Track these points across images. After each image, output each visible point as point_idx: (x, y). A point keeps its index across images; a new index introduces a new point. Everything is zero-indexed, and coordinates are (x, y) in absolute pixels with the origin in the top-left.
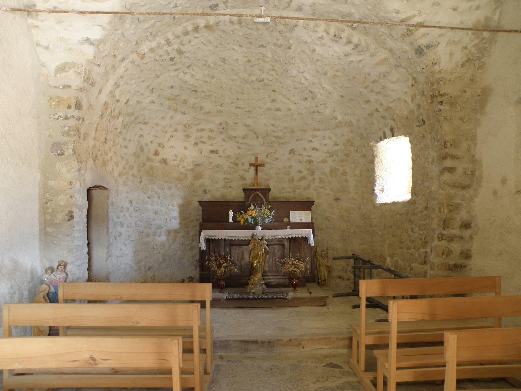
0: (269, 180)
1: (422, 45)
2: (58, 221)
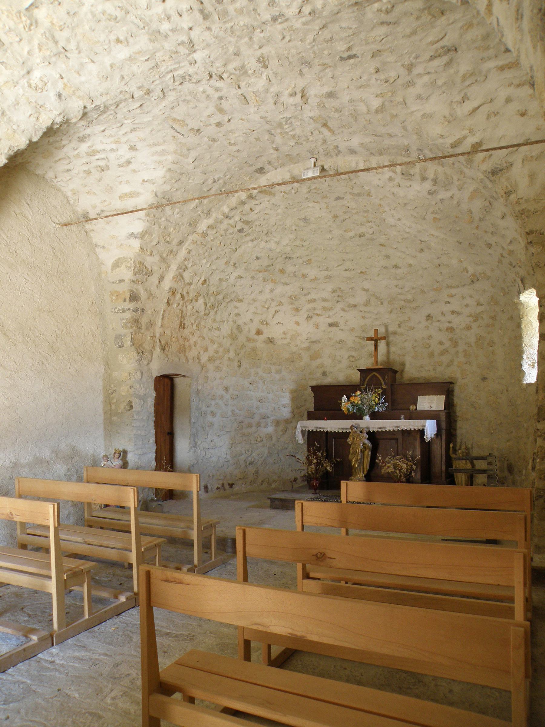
0: (404, 355)
2: (120, 411)
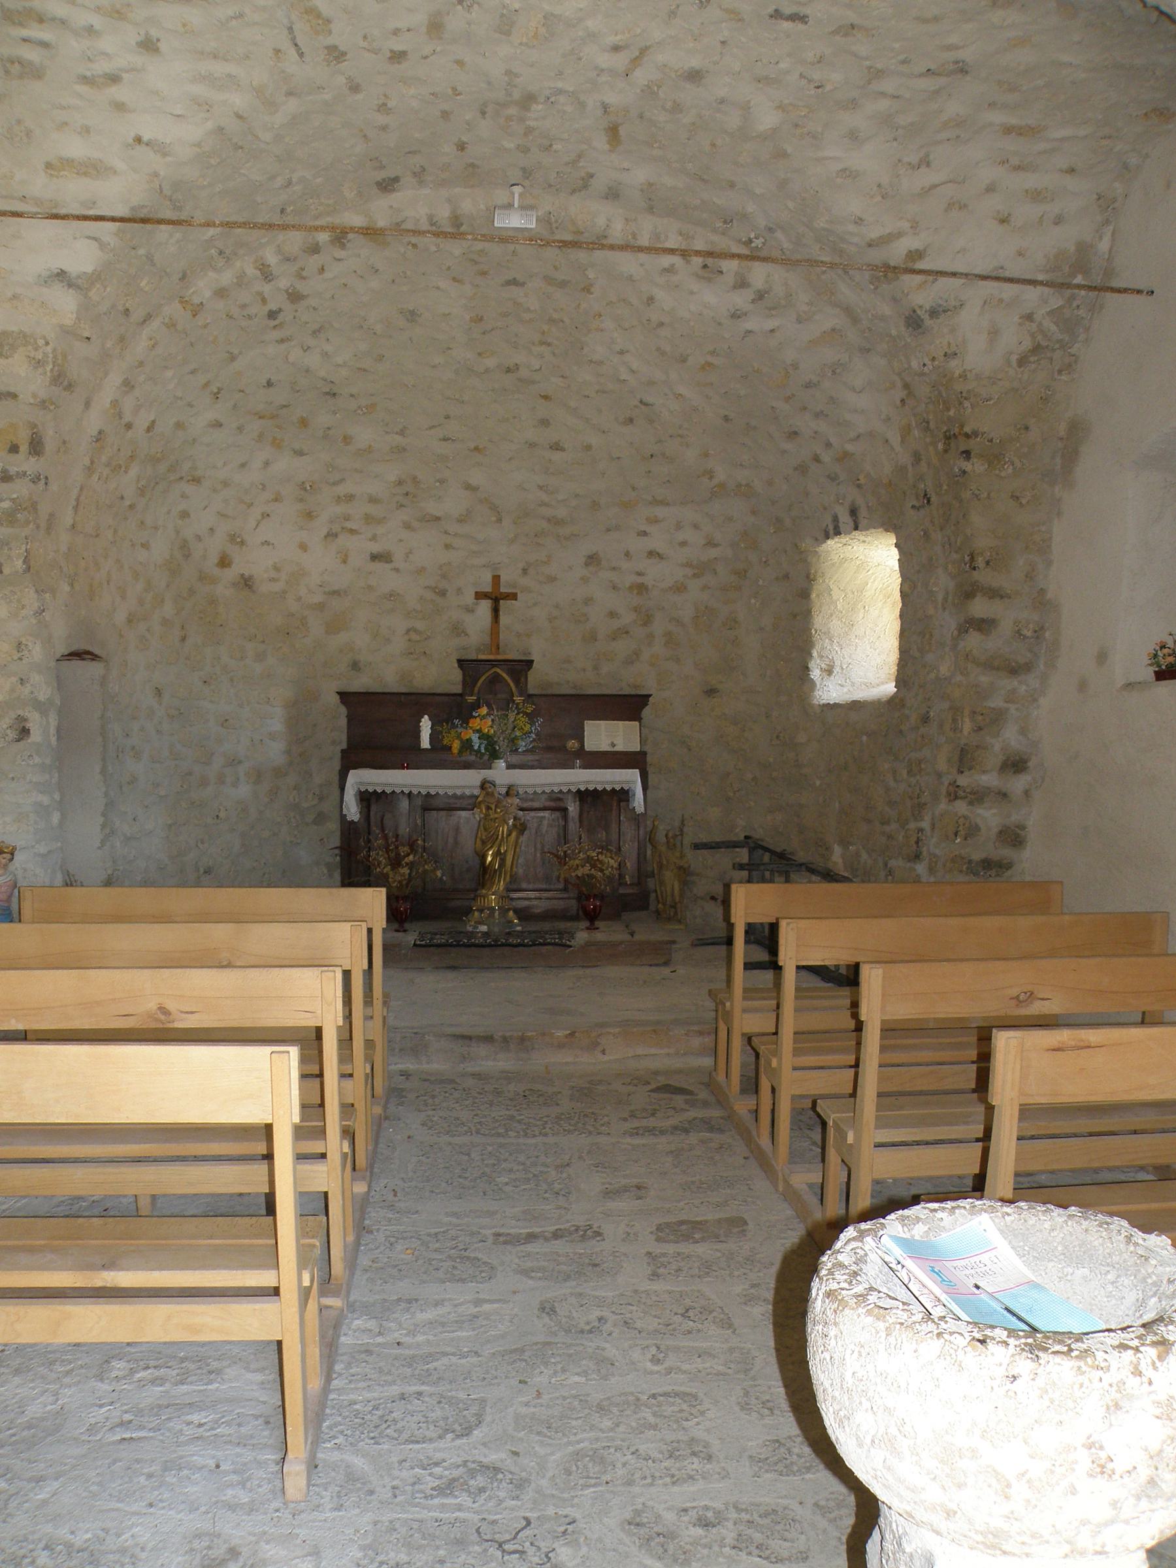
1: (921, 307)
